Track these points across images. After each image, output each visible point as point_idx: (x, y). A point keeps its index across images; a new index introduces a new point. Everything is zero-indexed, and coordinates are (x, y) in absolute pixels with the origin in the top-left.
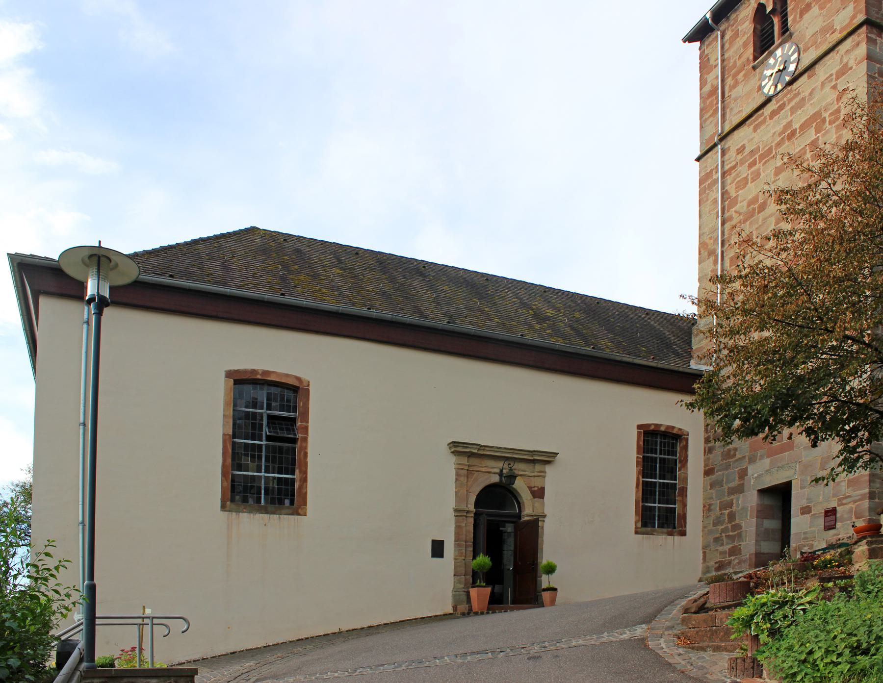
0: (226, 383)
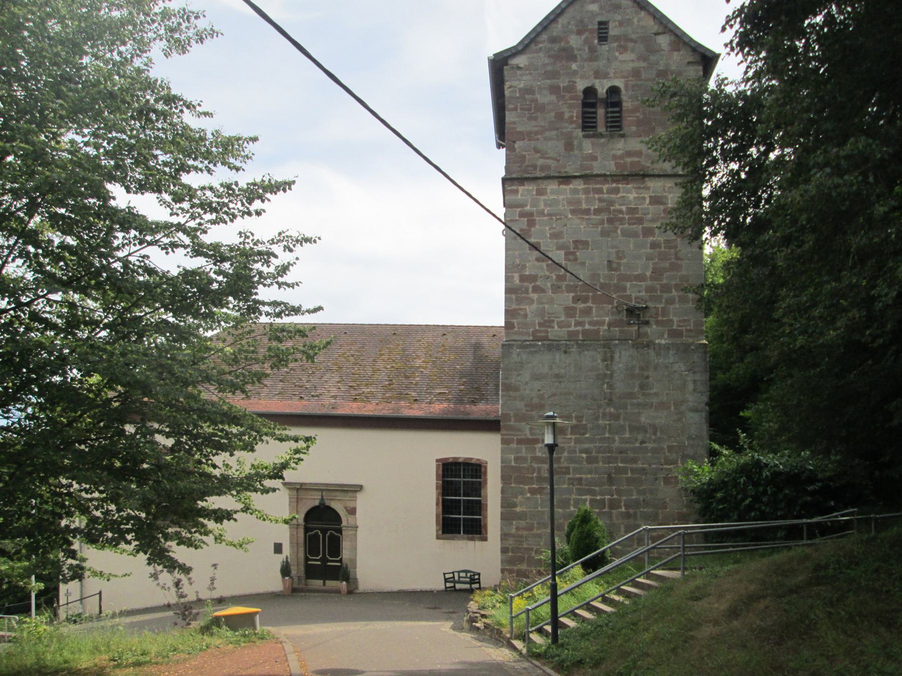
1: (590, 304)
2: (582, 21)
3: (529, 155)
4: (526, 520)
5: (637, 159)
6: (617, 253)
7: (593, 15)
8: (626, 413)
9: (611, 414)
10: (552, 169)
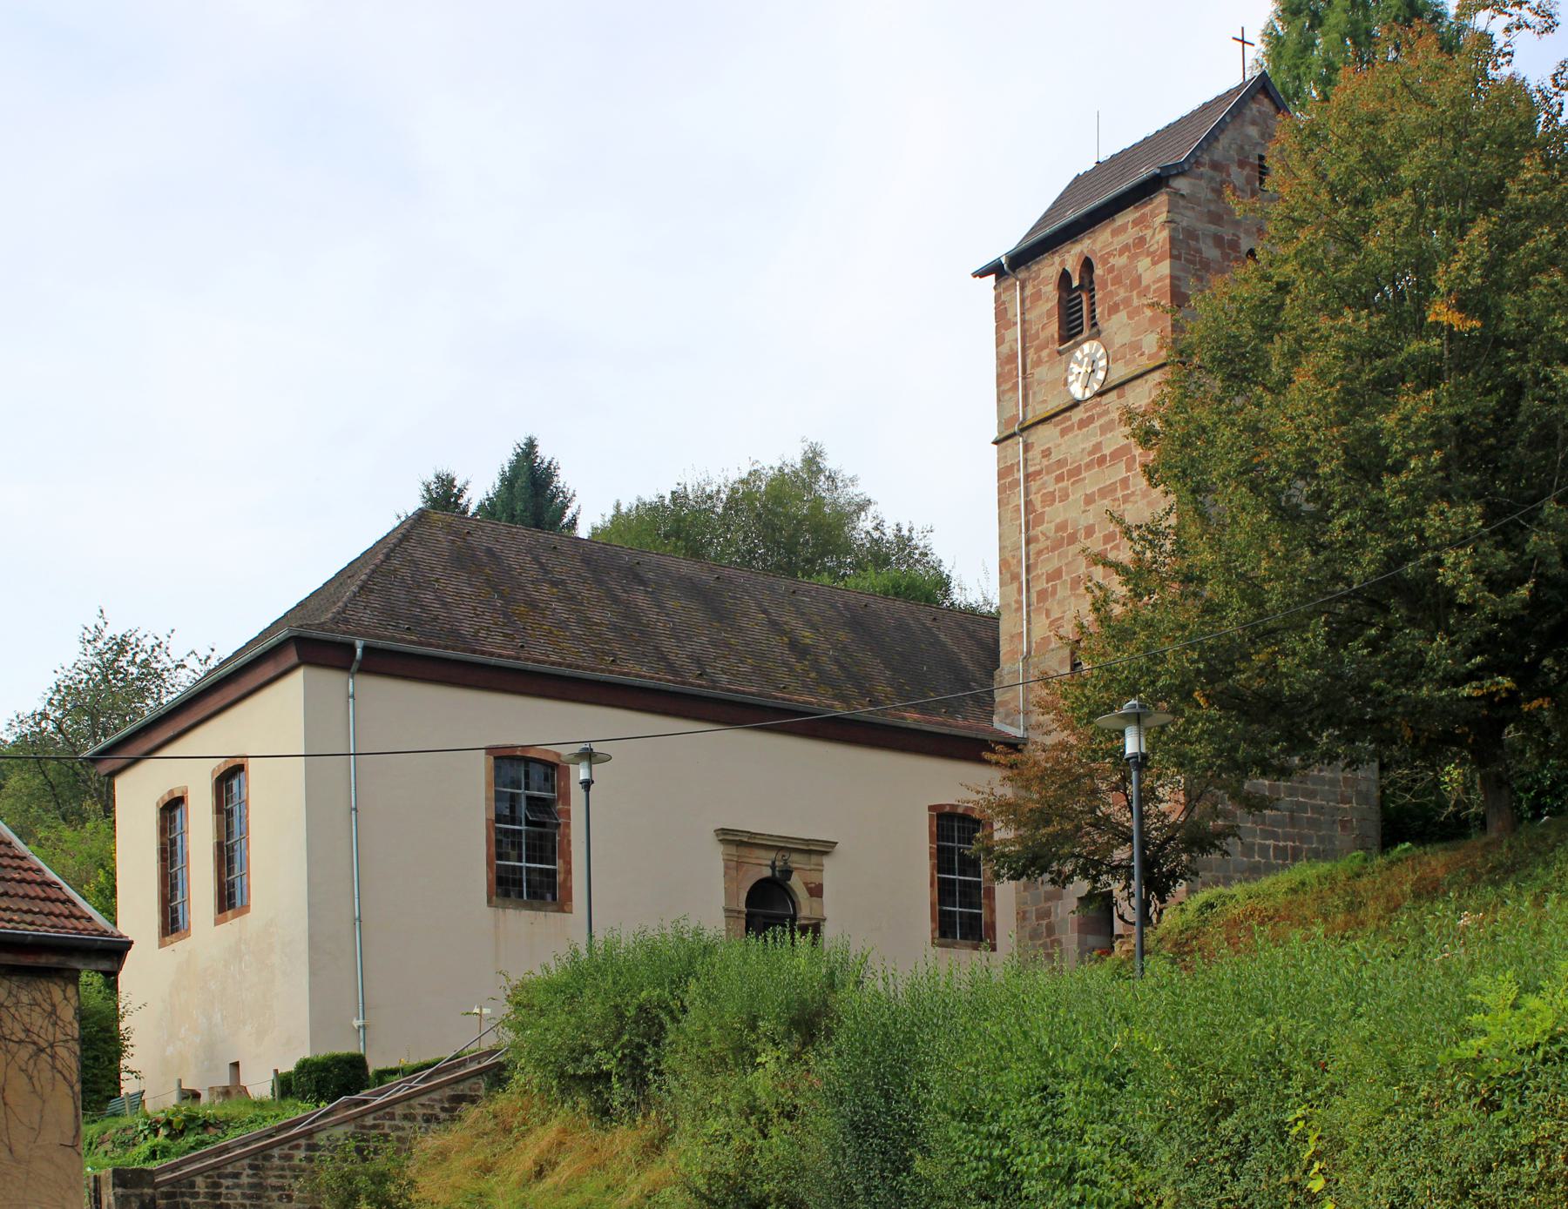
0: (486, 759)
2: (1242, 148)
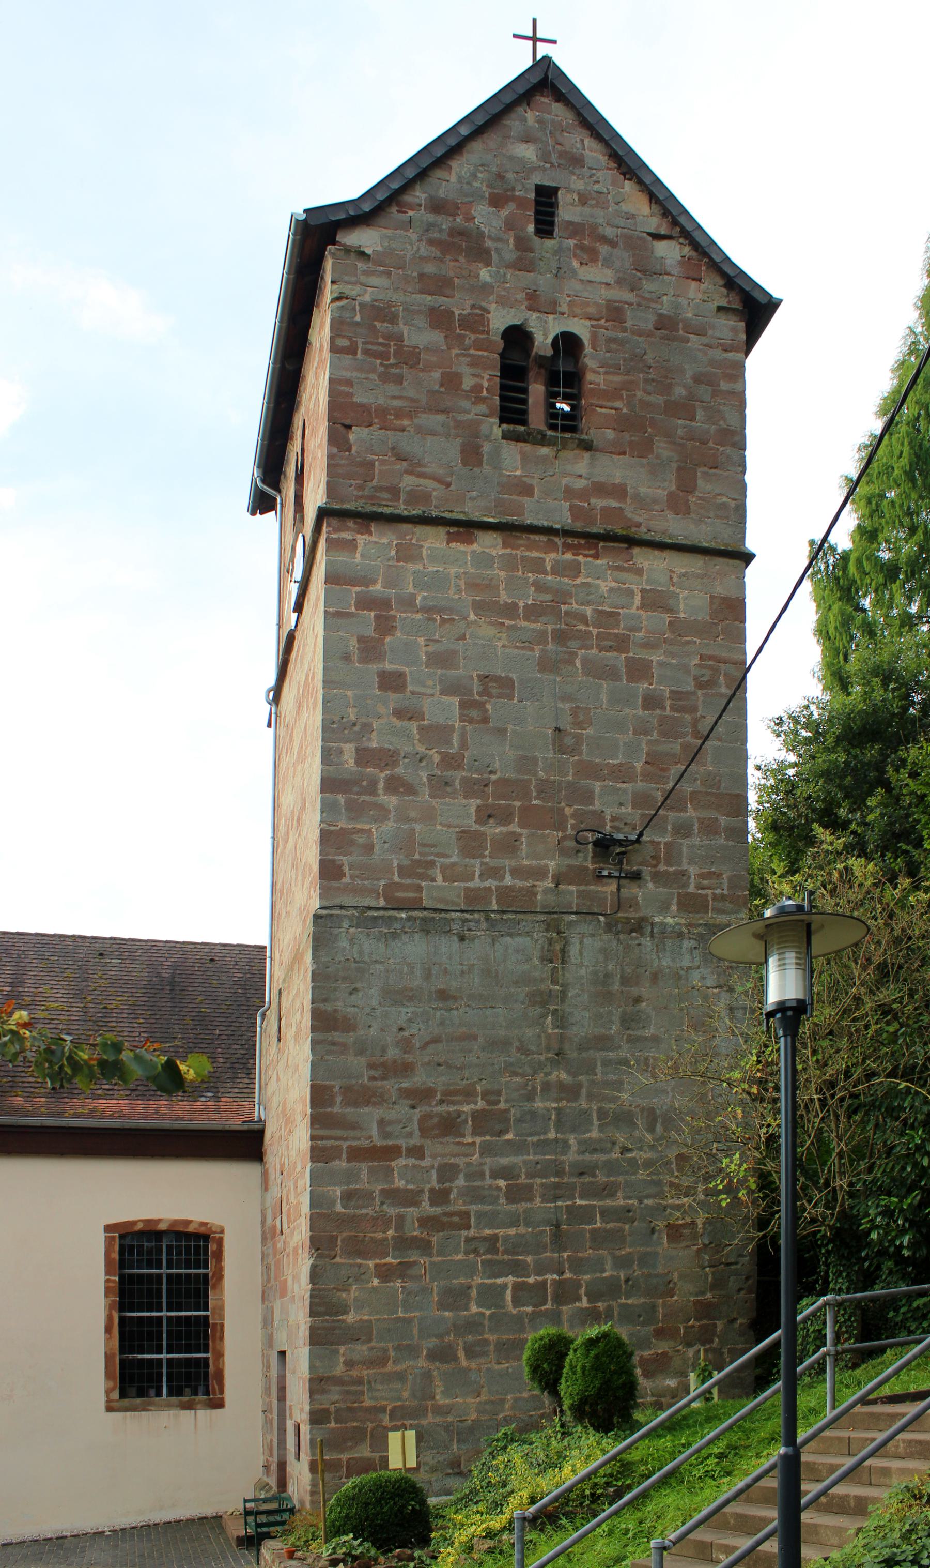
1: (514, 828)
2: (500, 176)
3: (382, 462)
4: (369, 1340)
5: (614, 504)
6: (575, 712)
7: (526, 169)
8: (593, 1082)
9: (561, 1086)
10: (434, 502)
